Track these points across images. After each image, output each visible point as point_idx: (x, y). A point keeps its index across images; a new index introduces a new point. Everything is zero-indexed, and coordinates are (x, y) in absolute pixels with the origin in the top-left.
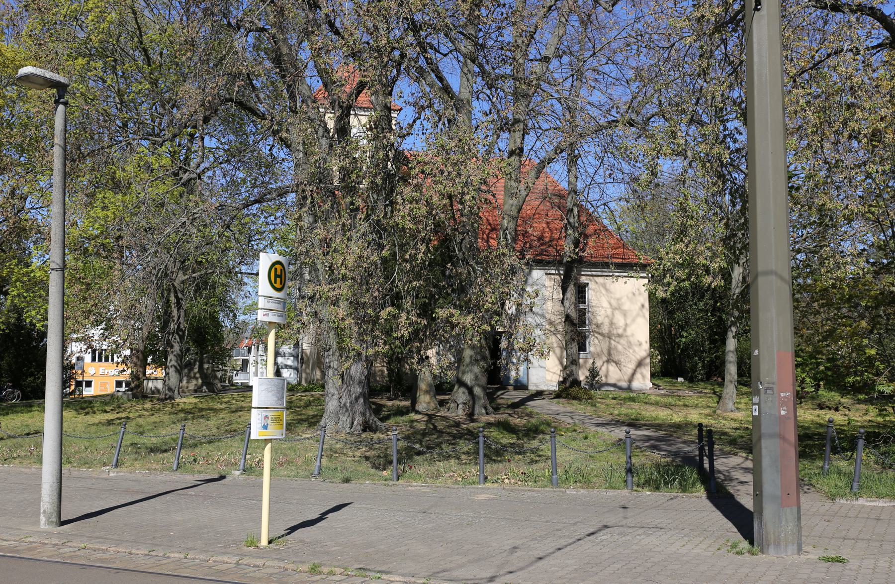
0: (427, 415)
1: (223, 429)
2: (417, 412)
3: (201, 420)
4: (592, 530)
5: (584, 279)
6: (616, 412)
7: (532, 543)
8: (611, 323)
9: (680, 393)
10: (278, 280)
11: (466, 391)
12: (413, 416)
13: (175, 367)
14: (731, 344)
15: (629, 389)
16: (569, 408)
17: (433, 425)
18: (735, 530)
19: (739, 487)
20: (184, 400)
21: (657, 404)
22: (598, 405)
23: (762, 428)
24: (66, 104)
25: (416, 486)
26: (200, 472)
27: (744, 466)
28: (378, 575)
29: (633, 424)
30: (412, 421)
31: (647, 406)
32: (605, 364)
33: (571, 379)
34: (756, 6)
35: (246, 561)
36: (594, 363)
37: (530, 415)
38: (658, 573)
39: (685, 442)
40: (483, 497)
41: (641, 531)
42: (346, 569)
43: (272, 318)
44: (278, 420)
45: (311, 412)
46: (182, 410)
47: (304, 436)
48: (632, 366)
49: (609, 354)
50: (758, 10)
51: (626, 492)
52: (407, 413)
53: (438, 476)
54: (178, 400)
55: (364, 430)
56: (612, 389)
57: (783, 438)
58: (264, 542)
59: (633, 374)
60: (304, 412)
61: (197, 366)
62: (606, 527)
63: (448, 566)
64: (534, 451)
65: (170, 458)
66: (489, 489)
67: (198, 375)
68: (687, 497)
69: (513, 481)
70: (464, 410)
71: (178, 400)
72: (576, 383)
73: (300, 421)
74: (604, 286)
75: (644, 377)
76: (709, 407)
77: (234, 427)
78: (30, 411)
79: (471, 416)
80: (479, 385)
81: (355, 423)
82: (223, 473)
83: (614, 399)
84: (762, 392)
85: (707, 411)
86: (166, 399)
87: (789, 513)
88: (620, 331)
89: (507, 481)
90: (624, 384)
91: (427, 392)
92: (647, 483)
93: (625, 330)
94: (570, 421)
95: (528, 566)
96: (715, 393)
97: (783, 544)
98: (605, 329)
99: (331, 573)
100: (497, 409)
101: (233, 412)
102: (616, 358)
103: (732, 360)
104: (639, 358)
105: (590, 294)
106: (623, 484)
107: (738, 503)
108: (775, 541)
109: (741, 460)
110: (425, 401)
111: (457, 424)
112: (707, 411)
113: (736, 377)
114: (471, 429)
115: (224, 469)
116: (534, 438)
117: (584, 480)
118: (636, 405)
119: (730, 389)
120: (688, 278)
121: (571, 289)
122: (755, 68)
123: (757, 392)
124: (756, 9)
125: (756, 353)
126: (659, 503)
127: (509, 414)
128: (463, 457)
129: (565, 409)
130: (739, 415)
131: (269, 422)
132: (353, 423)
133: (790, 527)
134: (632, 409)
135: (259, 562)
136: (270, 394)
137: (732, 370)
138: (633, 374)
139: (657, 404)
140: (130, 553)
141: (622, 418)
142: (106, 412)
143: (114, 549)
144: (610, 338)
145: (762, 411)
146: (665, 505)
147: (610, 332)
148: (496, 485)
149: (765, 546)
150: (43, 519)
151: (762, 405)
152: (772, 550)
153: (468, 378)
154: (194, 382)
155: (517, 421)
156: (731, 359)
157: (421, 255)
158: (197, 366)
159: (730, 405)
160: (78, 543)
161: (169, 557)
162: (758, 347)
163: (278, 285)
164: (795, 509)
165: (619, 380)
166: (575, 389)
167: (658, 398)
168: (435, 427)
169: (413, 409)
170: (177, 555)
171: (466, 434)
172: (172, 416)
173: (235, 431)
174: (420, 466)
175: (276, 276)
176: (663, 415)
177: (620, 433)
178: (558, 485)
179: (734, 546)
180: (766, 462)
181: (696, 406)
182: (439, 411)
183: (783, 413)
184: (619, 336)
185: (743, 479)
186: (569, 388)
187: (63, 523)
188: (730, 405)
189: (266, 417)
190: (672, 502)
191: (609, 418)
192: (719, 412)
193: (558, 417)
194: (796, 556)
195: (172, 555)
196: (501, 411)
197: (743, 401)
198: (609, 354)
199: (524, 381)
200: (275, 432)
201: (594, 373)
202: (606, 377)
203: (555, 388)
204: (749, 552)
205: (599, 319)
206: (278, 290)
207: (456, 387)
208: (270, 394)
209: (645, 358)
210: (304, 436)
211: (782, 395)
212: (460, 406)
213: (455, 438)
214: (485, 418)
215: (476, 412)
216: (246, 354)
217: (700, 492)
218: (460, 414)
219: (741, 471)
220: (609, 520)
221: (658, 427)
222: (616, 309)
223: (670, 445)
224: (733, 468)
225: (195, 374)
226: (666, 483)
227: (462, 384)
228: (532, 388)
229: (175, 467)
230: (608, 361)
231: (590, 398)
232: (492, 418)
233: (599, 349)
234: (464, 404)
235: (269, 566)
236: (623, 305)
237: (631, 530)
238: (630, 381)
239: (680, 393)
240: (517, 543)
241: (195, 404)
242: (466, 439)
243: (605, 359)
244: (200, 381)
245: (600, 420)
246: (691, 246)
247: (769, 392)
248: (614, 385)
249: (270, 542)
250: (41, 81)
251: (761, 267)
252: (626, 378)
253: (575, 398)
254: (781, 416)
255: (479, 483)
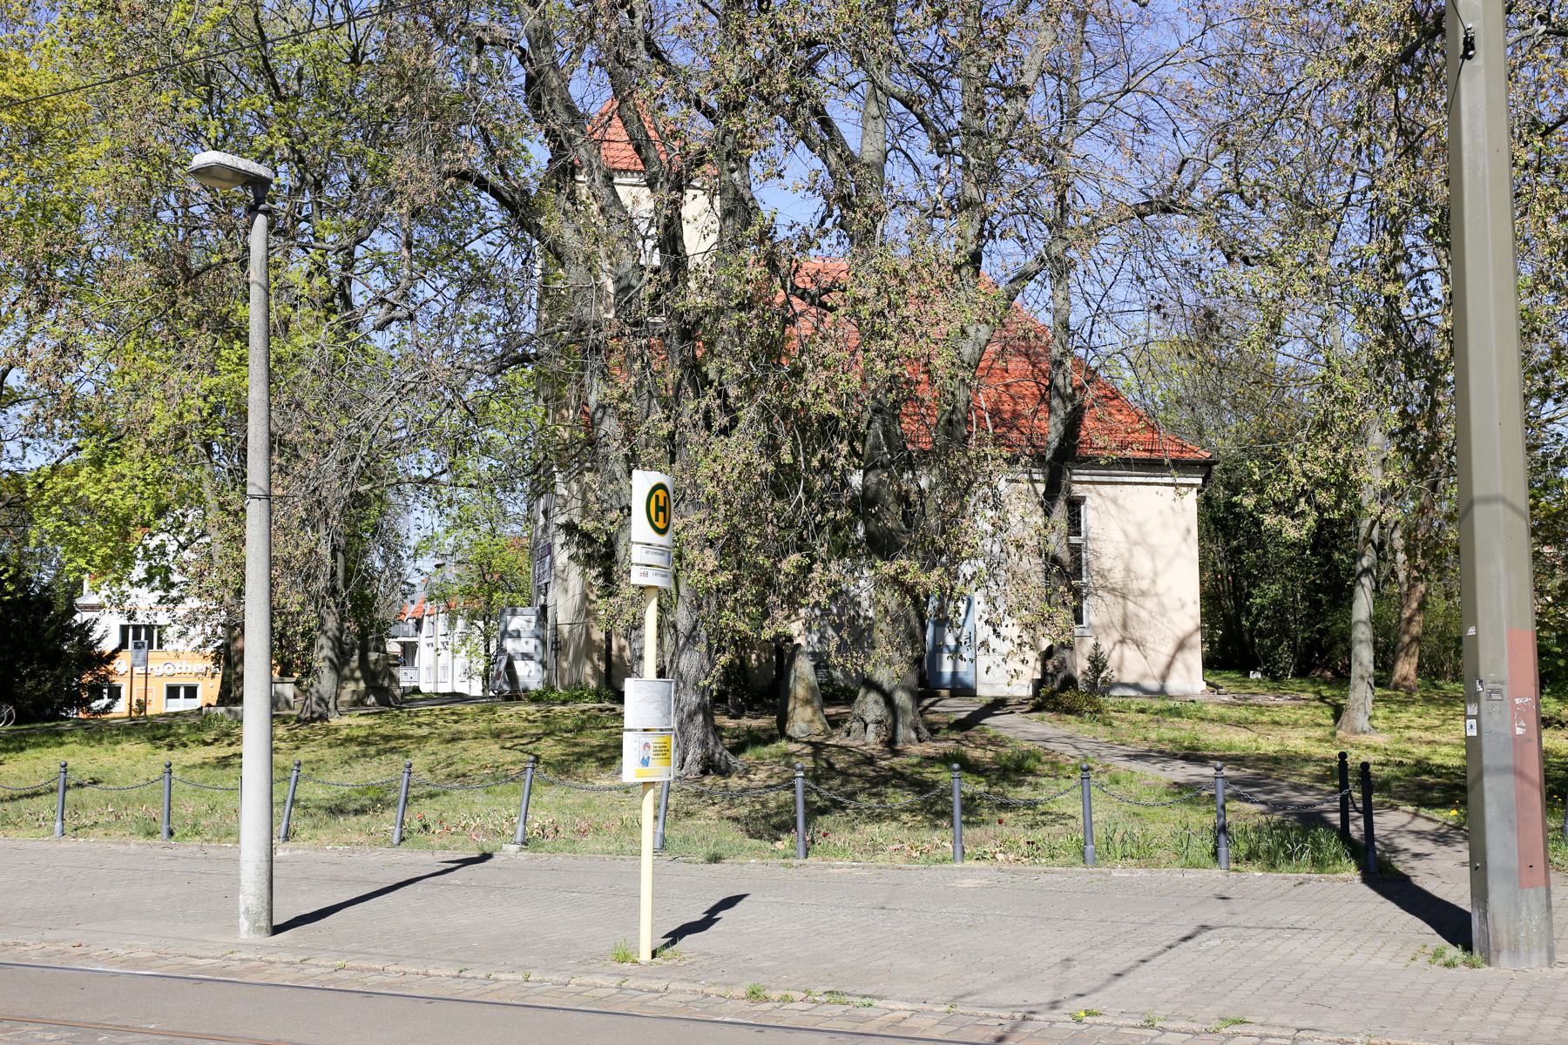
0: (809, 743)
1: (441, 773)
2: (790, 739)
3: (395, 757)
4: (1186, 933)
5: (1078, 490)
6: (1153, 736)
7: (1094, 952)
8: (1127, 570)
9: (1259, 699)
10: (661, 514)
11: (881, 700)
12: (783, 745)
13: (331, 660)
14: (1363, 605)
15: (1161, 693)
16: (1064, 730)
17: (827, 761)
18: (1432, 930)
19: (1415, 863)
20: (346, 720)
21: (1222, 720)
22: (1116, 723)
23: (1485, 756)
24: (267, 212)
25: (841, 867)
26: (444, 848)
27: (1411, 827)
28: (866, 1001)
29: (1193, 756)
30: (788, 755)
31: (1205, 725)
32: (1118, 647)
33: (1061, 676)
34: (1466, 51)
35: (632, 983)
36: (1096, 646)
37: (995, 741)
38: (1326, 994)
39: (1296, 788)
40: (968, 883)
41: (1270, 933)
42: (808, 992)
43: (654, 579)
44: (663, 751)
45: (594, 739)
46: (350, 740)
47: (597, 783)
48: (1168, 648)
49: (1125, 626)
50: (1470, 58)
51: (1216, 873)
52: (772, 739)
53: (875, 848)
54: (335, 721)
55: (705, 772)
56: (1132, 693)
57: (1519, 773)
58: (645, 956)
59: (1169, 666)
60: (579, 740)
61: (356, 657)
62: (1205, 928)
63: (971, 987)
64: (1031, 805)
65: (388, 822)
66: (973, 870)
67: (358, 674)
68: (1327, 880)
69: (1011, 857)
70: (878, 735)
71: (335, 721)
72: (1070, 682)
73: (580, 758)
74: (1114, 501)
75: (1188, 669)
76: (1320, 725)
77: (460, 768)
78: (62, 744)
79: (891, 743)
80: (903, 688)
81: (689, 758)
82: (487, 850)
83: (1142, 711)
84: (1483, 696)
85: (1319, 733)
86: (314, 720)
87: (1534, 897)
88: (1145, 585)
89: (1000, 856)
90: (1153, 685)
91: (807, 702)
92: (1252, 856)
93: (1154, 582)
94: (1074, 752)
95: (1104, 986)
96: (1322, 699)
97: (1523, 948)
98: (1117, 577)
99: (786, 999)
100: (933, 730)
101: (448, 742)
102: (1137, 634)
103: (1363, 637)
104: (1181, 634)
105: (1088, 516)
106: (1210, 860)
107: (1419, 889)
108: (1509, 944)
109: (1407, 818)
110: (803, 719)
111: (870, 760)
112: (1319, 733)
113: (1371, 669)
114: (899, 769)
115: (488, 845)
116: (1020, 784)
117: (1142, 853)
118: (1185, 723)
119: (1361, 693)
120: (1337, 505)
121: (1060, 511)
122: (1465, 155)
123: (1474, 697)
124: (1466, 56)
125: (1471, 631)
126: (1281, 890)
127: (958, 741)
128: (905, 817)
129: (1057, 731)
130: (1380, 740)
131: (651, 753)
132: (684, 760)
133: (1533, 920)
134: (1180, 729)
135: (660, 985)
136: (652, 707)
137: (1364, 656)
138: (1169, 666)
139: (1222, 720)
140: (426, 975)
141: (1168, 748)
142: (206, 744)
143: (396, 968)
144: (1124, 597)
145: (1484, 728)
146: (1293, 893)
147: (1125, 585)
148: (983, 864)
149: (1493, 953)
150: (244, 924)
151: (1484, 719)
152: (1504, 959)
153: (883, 676)
154: (351, 686)
155: (978, 753)
156: (1362, 634)
157: (842, 460)
158: (356, 657)
159: (1362, 722)
160: (314, 956)
161: (496, 980)
162: (1474, 622)
163: (661, 525)
164: (1542, 891)
165: (1145, 676)
166: (1066, 697)
167: (1223, 710)
168: (831, 766)
169: (781, 732)
170: (510, 976)
171: (893, 777)
172: (337, 750)
173: (464, 775)
174: (837, 832)
175: (659, 509)
176: (1241, 740)
177: (1182, 772)
178: (1095, 864)
179: (1438, 954)
180: (1492, 812)
181: (1295, 725)
182: (831, 736)
183: (1519, 731)
184: (1143, 594)
185: (1416, 849)
186: (1059, 691)
187: (276, 930)
188: (1362, 722)
189: (647, 745)
190: (1302, 888)
191: (1144, 747)
192: (1340, 733)
193: (1048, 745)
194: (1546, 970)
195: (502, 976)
196: (939, 736)
197: (1379, 713)
198: (1125, 626)
199: (969, 679)
200: (661, 771)
201: (1097, 663)
202: (1119, 670)
203: (1027, 692)
204: (1464, 963)
205: (1106, 563)
206: (662, 532)
207: (862, 692)
208: (652, 707)
209: (1191, 635)
210: (597, 783)
211: (1517, 701)
212: (871, 727)
213: (875, 785)
214: (916, 749)
215: (900, 738)
216: (412, 631)
217: (1350, 872)
218: (871, 741)
219: (1412, 837)
220: (1210, 917)
221: (1238, 761)
222: (1136, 544)
223: (1271, 792)
224: (1395, 831)
225: (353, 671)
226: (1289, 857)
227: (872, 685)
228: (986, 692)
229: (396, 839)
230: (1122, 641)
231: (1099, 711)
232: (930, 748)
233: (1106, 619)
234: (879, 723)
235: (676, 991)
236: (1150, 538)
237: (1251, 932)
238: (1164, 678)
239: (1259, 699)
240: (1068, 953)
241: (371, 727)
242: (894, 786)
243: (1116, 636)
244: (362, 685)
245: (1130, 750)
246: (1343, 451)
247: (1494, 696)
248: (1136, 686)
249: (654, 954)
250: (228, 175)
251: (1478, 491)
252: (1157, 671)
253: (1069, 711)
254: (1516, 738)
255: (954, 860)
